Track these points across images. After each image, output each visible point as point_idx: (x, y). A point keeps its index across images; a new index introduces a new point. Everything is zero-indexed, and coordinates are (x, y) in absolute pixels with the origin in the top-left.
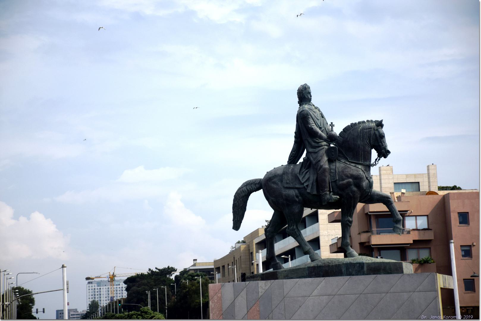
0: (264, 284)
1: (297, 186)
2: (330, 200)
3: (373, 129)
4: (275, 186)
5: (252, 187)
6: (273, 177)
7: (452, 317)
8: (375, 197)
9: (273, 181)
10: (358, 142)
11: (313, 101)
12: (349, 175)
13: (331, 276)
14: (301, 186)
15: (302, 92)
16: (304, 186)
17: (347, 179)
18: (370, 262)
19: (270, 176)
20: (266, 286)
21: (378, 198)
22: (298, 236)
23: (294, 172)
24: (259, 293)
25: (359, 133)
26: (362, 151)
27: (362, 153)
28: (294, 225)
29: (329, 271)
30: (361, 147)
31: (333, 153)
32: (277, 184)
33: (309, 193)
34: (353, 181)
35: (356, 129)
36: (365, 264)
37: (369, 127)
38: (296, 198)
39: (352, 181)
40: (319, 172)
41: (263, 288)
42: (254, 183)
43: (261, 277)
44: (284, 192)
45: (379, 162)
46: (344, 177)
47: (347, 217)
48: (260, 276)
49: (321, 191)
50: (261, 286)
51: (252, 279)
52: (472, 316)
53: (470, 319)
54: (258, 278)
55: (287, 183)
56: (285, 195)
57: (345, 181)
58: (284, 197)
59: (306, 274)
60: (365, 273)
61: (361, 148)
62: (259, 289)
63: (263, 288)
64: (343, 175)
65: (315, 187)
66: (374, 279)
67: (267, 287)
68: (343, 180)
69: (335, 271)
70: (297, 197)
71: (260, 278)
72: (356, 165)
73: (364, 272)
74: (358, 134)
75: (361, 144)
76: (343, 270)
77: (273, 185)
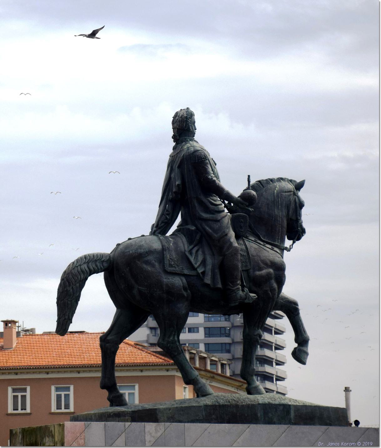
0: (154, 429)
1: (186, 272)
2: (246, 299)
3: (292, 193)
4: (149, 268)
5: (96, 266)
6: (147, 252)
7: (350, 444)
8: (280, 300)
9: (146, 259)
10: (275, 210)
11: (196, 138)
12: (269, 263)
13: (241, 423)
14: (193, 273)
15: (187, 121)
16: (198, 273)
17: (266, 268)
18: (301, 404)
19: (139, 250)
20: (156, 431)
21: (282, 303)
22: (181, 353)
23: (179, 249)
24: (146, 442)
25: (276, 197)
26: (280, 226)
27: (279, 229)
28: (174, 335)
29: (238, 414)
30: (278, 219)
31: (242, 224)
32: (153, 266)
33: (207, 285)
34: (274, 273)
35: (270, 189)
36: (292, 407)
37: (289, 190)
38: (183, 291)
39: (273, 273)
40: (228, 253)
41: (152, 435)
42: (100, 259)
43: (131, 416)
44: (165, 280)
45: (293, 245)
46: (262, 265)
47: (258, 329)
48: (129, 414)
49: (230, 284)
50: (149, 432)
51: (117, 419)
52: (371, 443)
53: (370, 446)
54: (127, 418)
55: (171, 266)
56: (167, 285)
57: (264, 272)
58: (164, 287)
59: (202, 416)
60: (293, 422)
61: (279, 221)
62: (146, 435)
63: (152, 435)
64: (260, 262)
65: (218, 276)
66: (324, 433)
67: (159, 434)
68: (260, 269)
69: (246, 415)
70: (185, 289)
71: (130, 418)
72: (274, 247)
73: (290, 419)
74: (275, 199)
75: (279, 214)
76: (259, 415)
77: (145, 266)
